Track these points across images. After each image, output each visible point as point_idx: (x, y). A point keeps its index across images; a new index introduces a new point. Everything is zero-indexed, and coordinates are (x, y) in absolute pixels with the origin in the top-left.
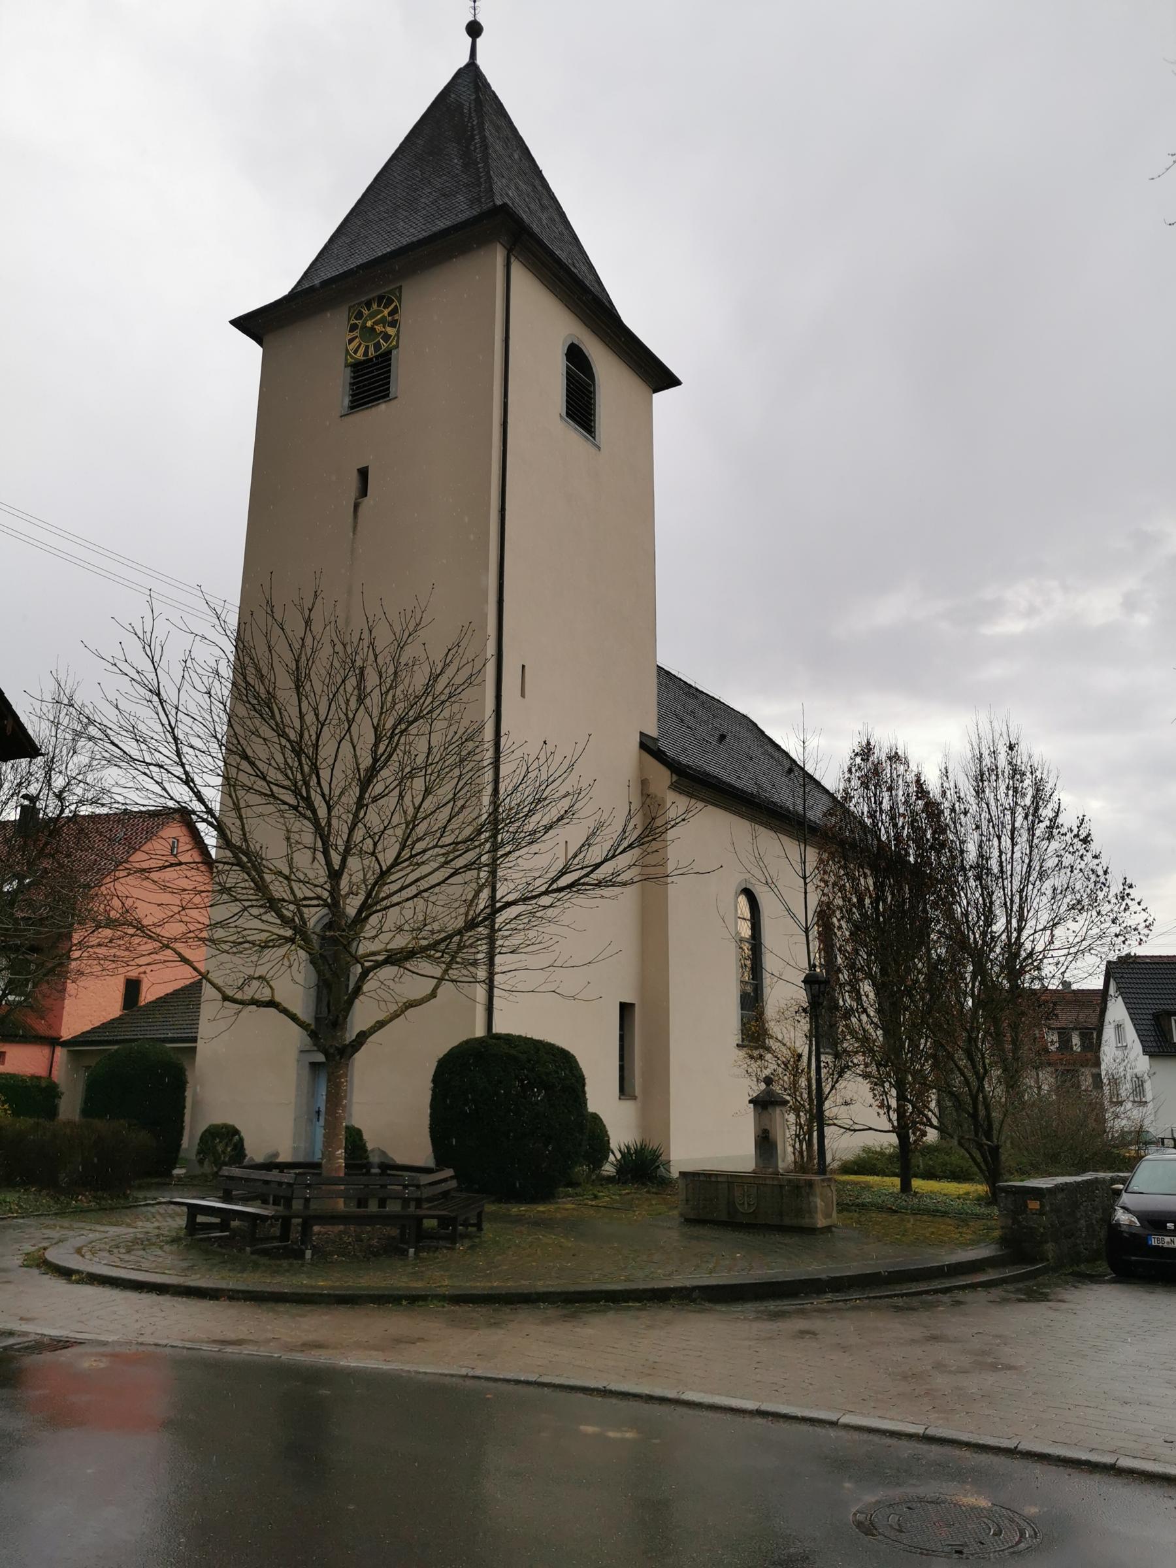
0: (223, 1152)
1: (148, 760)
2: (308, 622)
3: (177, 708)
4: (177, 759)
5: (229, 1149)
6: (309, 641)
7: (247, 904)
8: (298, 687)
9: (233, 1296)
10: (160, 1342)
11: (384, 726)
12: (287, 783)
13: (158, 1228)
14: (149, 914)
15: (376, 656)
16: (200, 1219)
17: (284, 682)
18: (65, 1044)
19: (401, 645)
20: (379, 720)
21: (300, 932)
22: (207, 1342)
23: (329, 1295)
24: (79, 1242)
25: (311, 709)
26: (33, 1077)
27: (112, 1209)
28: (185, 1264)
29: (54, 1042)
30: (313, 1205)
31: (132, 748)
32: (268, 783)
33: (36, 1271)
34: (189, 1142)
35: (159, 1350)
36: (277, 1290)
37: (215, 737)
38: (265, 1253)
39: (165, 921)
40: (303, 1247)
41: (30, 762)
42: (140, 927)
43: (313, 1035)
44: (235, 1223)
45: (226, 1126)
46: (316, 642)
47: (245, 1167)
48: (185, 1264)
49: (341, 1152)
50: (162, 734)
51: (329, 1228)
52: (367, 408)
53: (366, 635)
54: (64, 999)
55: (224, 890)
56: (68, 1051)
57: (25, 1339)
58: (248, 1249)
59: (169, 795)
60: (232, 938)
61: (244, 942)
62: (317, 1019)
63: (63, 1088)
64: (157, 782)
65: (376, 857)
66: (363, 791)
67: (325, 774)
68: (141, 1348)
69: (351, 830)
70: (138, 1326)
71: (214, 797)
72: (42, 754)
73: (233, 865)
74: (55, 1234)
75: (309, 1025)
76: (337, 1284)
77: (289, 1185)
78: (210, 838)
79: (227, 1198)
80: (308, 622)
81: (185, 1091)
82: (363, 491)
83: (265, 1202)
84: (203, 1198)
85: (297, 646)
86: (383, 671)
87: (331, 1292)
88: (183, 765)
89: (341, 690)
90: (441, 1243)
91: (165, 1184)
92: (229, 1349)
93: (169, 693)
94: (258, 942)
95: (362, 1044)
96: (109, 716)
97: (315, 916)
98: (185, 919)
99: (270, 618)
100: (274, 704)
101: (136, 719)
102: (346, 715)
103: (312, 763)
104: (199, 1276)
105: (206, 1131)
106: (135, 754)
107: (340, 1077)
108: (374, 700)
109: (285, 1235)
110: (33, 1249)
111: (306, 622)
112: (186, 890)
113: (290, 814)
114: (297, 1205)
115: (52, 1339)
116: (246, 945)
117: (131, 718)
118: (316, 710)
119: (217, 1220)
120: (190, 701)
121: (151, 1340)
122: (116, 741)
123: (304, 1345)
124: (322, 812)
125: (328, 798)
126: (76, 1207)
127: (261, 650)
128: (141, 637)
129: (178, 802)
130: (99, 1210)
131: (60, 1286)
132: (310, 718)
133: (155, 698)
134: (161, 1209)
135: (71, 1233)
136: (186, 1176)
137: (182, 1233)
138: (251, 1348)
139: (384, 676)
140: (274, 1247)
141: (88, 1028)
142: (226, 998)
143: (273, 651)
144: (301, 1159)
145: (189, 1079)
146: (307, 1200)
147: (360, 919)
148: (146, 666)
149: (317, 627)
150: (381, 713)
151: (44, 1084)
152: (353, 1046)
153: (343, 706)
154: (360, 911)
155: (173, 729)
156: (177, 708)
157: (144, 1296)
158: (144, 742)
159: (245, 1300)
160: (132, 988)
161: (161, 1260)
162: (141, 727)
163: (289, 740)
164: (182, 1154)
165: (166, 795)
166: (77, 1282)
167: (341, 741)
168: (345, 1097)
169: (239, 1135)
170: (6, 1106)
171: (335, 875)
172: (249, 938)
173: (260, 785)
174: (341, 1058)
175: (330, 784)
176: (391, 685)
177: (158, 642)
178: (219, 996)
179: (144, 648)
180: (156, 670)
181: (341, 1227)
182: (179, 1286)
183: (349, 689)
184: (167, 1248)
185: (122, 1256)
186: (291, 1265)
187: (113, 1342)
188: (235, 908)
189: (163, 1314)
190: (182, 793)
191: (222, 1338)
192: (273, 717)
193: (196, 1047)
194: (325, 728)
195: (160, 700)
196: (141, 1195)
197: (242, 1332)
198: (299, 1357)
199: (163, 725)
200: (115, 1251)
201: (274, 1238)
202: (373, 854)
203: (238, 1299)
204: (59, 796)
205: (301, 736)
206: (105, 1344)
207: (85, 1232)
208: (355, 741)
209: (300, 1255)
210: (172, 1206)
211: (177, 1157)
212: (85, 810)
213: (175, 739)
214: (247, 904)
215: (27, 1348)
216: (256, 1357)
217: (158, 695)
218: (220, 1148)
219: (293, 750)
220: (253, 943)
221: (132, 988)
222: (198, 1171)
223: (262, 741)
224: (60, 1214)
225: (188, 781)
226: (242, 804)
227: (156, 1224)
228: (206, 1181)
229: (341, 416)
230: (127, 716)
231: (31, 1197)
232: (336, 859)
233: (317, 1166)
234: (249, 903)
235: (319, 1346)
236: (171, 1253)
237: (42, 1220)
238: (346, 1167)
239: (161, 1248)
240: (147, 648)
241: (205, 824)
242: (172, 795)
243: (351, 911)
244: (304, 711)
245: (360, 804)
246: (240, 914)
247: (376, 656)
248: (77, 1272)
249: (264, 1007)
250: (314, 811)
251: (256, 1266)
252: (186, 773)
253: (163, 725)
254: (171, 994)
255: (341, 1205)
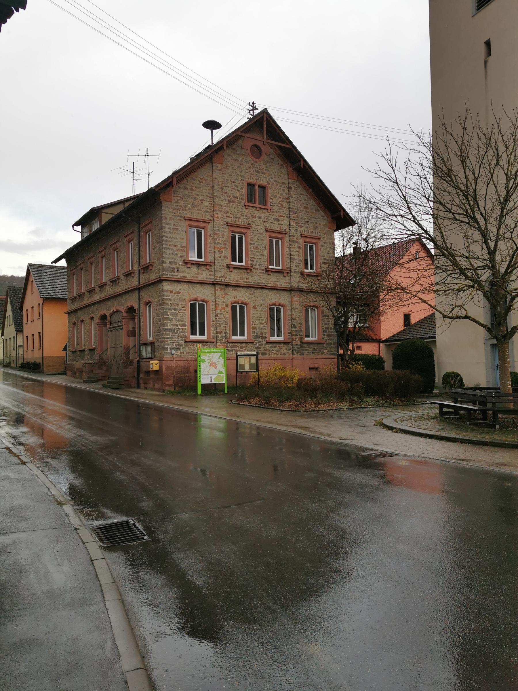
0: (454, 383)
1: (396, 214)
2: (464, 128)
3: (405, 187)
4: (408, 211)
5: (456, 382)
6: (466, 138)
7: (449, 273)
8: (463, 162)
9: (462, 441)
10: (431, 457)
11: (511, 173)
12: (462, 212)
13: (428, 413)
14: (406, 283)
15: (502, 136)
16: (445, 410)
17: (456, 162)
18: (383, 342)
19: (516, 127)
20: (508, 170)
21: (477, 282)
22: (452, 459)
23: (509, 444)
24: (396, 417)
25: (471, 172)
26: (373, 355)
27: (408, 405)
28: (440, 428)
29: (379, 341)
30: (497, 405)
31: (389, 211)
32: (453, 214)
33: (379, 427)
34: (438, 380)
35: (431, 460)
36: (482, 440)
37: (425, 197)
38: (476, 425)
39: (412, 285)
40: (495, 423)
41: (353, 228)
42: (403, 289)
43: (488, 330)
44: (462, 412)
45: (453, 373)
46: (469, 138)
47: (465, 389)
48: (440, 428)
49: (509, 383)
50: (400, 201)
51: (506, 416)
52: (486, 6)
53: (496, 126)
54: (380, 323)
55: (437, 268)
56: (385, 344)
57: (377, 452)
58: (468, 423)
59: (407, 229)
60: (443, 289)
61: (449, 290)
62: (492, 324)
63: (385, 359)
64: (402, 224)
65: (513, 240)
66: (502, 209)
67: (481, 204)
68: (423, 459)
69: (499, 229)
70: (421, 450)
71: (430, 227)
72: (356, 223)
73: (440, 256)
74: (386, 414)
75: (487, 325)
76: (513, 439)
77: (485, 397)
78: (430, 246)
79: (456, 401)
80: (464, 128)
81: (433, 358)
82: (489, 53)
83: (474, 403)
84: (445, 401)
85: (460, 142)
86: (507, 144)
87: (510, 443)
88: (411, 214)
89: (485, 158)
90: (313, 274)
91: (430, 396)
92: (462, 462)
93: (401, 181)
94: (456, 289)
95: (515, 332)
96: (377, 198)
97: (485, 275)
98: (422, 283)
99: (445, 131)
100: (452, 175)
101: (389, 197)
102: (490, 172)
103: (474, 199)
104: (446, 432)
105: (445, 375)
106: (391, 213)
107: (503, 348)
108: (504, 161)
109: (485, 418)
110: (378, 419)
111: (463, 129)
112: (420, 270)
113: (466, 227)
114: (489, 405)
115: (387, 453)
116: (450, 291)
117: (386, 197)
118: (474, 173)
119: (453, 411)
120: (411, 182)
121: (427, 456)
122: (382, 209)
123: (497, 464)
124: (482, 222)
125: (484, 215)
126: (394, 404)
127: (443, 149)
128: (386, 158)
129: (412, 231)
130: (404, 405)
131: (388, 433)
132: (471, 177)
133: (396, 184)
134: (429, 406)
135: (392, 414)
136: (439, 393)
137: (438, 415)
138: (471, 462)
139: (508, 146)
140: (481, 423)
141: (391, 335)
142: (445, 316)
143: (448, 148)
144: (491, 386)
145: (435, 353)
146: (494, 404)
147: (507, 273)
148: (389, 171)
149: (469, 129)
150: (509, 166)
151: (377, 358)
152: (510, 334)
153: (487, 167)
154: (507, 269)
155: (405, 197)
156: (405, 187)
157: (423, 439)
158: (394, 206)
159: (469, 443)
160: (407, 317)
161: (430, 425)
162: (391, 199)
163: (460, 190)
164: (436, 385)
165: (406, 229)
166: (396, 432)
167: (488, 185)
168: (509, 358)
169: (460, 376)
170: (364, 366)
171: (492, 253)
172: (451, 288)
173: (450, 215)
174: (504, 340)
175: (485, 208)
176: (513, 150)
177: (394, 158)
178: (441, 316)
179: (388, 163)
180: (394, 171)
181: (513, 416)
182: (437, 436)
183: (490, 157)
184: (432, 421)
185: (413, 423)
186: (489, 430)
187: (411, 456)
188: (444, 275)
189: (432, 446)
190: (413, 226)
191: (458, 458)
192: (452, 181)
193: (436, 341)
194: (478, 179)
195: (397, 184)
196: (420, 400)
197: (467, 456)
198: (494, 468)
199: (400, 196)
200: (410, 421)
201: (479, 419)
202: (511, 239)
203: (465, 443)
204: (366, 240)
205: (467, 186)
206: (408, 456)
207: (398, 414)
208: (496, 184)
209: (494, 427)
210: (433, 405)
211: (434, 385)
212: (377, 245)
213: (406, 201)
214: (449, 273)
215: (377, 455)
216: (474, 467)
217: (397, 183)
218: (452, 382)
219: (464, 195)
220: (453, 290)
221: (407, 317)
222: (444, 391)
223: (448, 194)
224: (388, 406)
225: (415, 220)
226: (442, 226)
227: (427, 411)
228: (448, 395)
229: (473, 17)
230: (384, 196)
231: (376, 400)
232: (492, 245)
233: (499, 389)
234: (450, 272)
235: (505, 465)
236: (434, 423)
237: (381, 409)
238: (513, 389)
239: (429, 420)
240: (389, 162)
241: (425, 239)
242: (409, 228)
243: (502, 270)
244: (467, 174)
245: (502, 216)
246: (446, 278)
247: (502, 136)
248: (395, 428)
249: (463, 319)
250: (478, 223)
251: (472, 430)
252: (413, 216)
253: (400, 196)
254: (423, 319)
255: (511, 406)
